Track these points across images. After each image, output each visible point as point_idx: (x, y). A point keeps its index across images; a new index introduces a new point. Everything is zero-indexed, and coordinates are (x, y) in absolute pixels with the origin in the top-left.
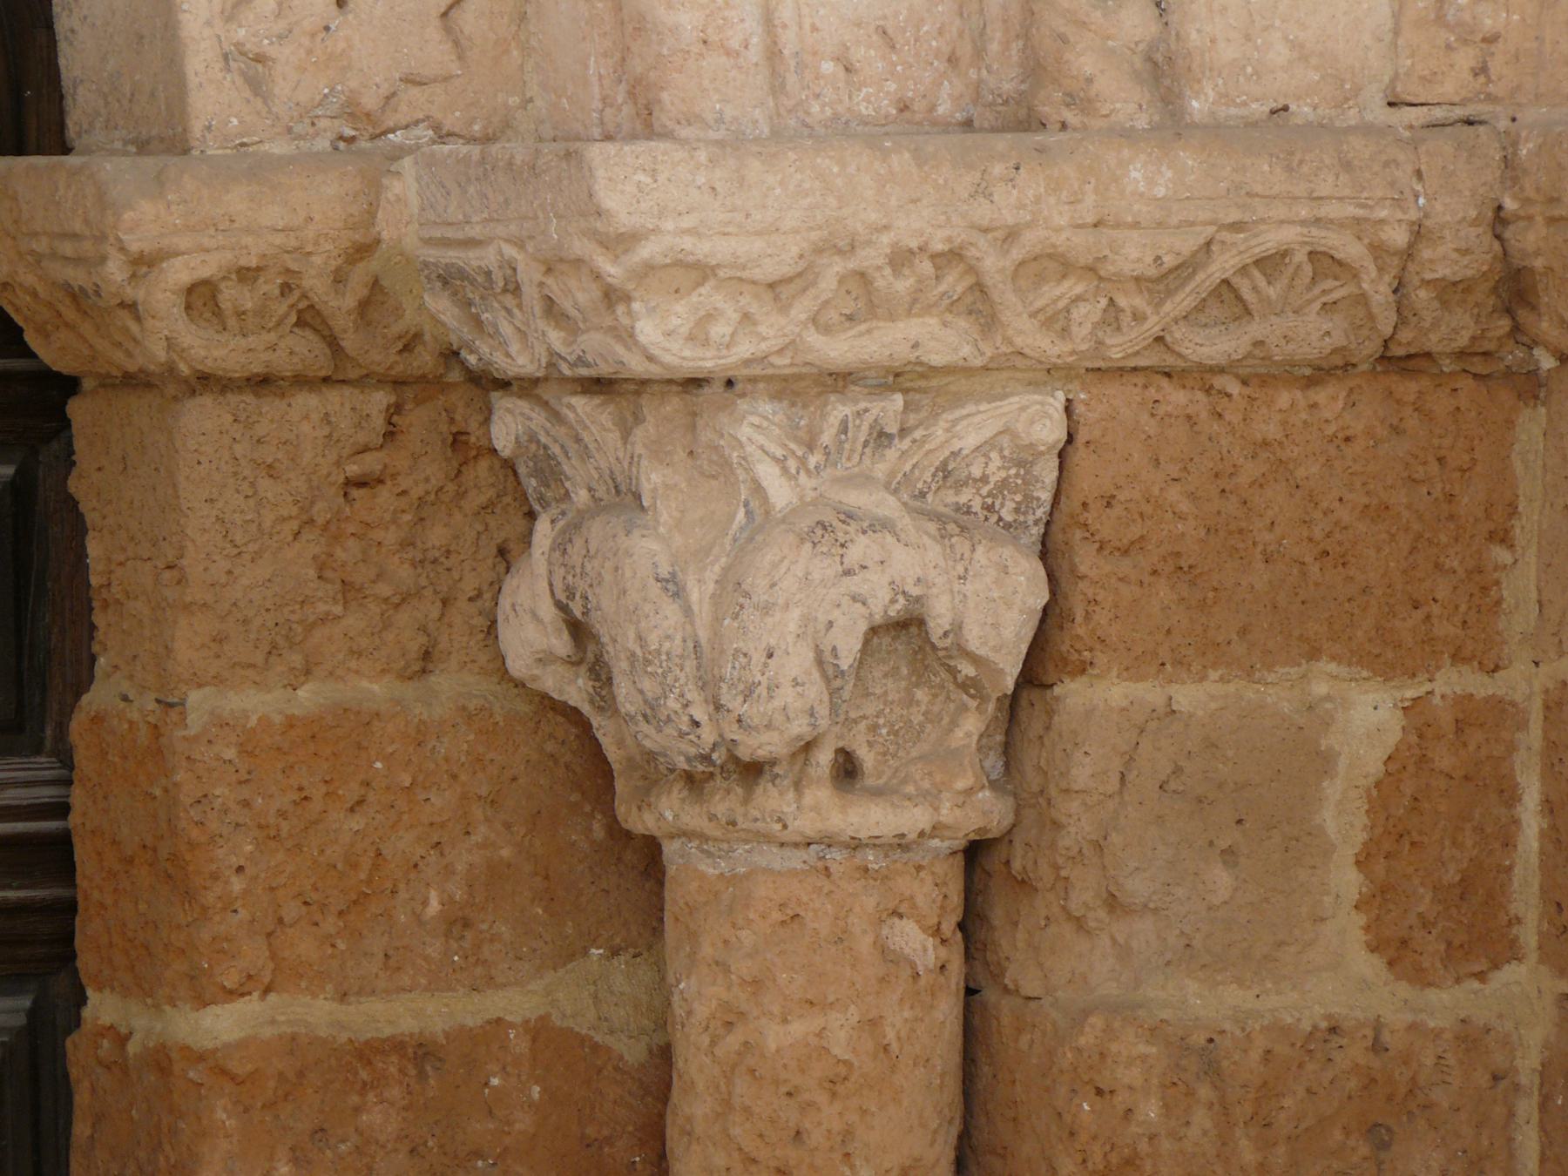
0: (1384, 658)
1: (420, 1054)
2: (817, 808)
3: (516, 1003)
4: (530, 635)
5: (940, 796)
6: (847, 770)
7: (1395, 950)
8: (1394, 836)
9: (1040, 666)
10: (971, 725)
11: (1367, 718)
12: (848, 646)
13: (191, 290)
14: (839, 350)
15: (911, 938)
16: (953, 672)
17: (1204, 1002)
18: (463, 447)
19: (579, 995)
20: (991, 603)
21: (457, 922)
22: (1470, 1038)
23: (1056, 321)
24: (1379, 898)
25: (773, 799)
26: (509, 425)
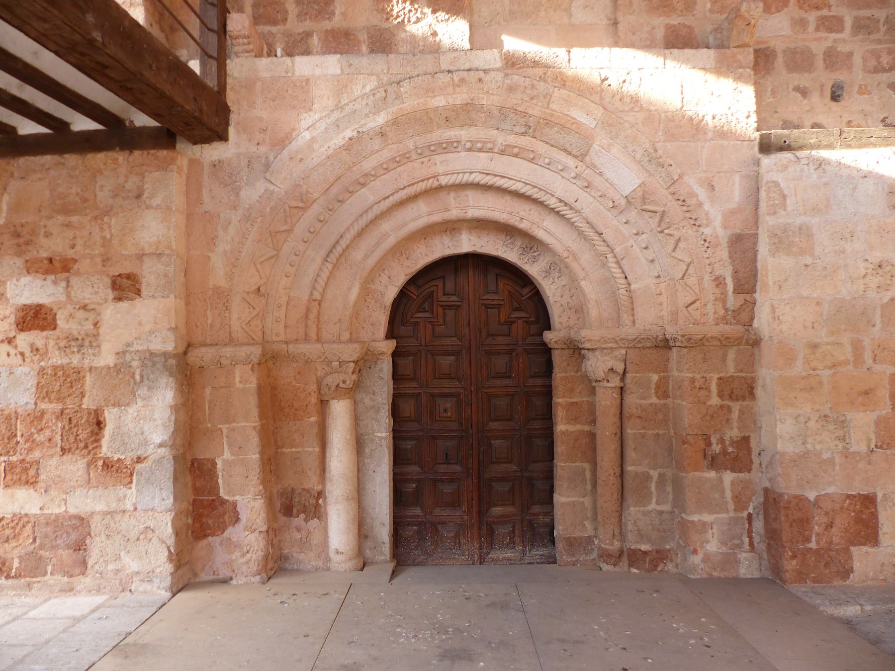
0: (656, 372)
1: (577, 403)
2: (606, 384)
3: (585, 399)
4: (583, 370)
5: (616, 382)
6: (608, 381)
7: (658, 398)
8: (658, 387)
9: (625, 373)
10: (619, 378)
11: (655, 378)
12: (606, 371)
13: (25, 308)
14: (603, 346)
15: (615, 395)
16: (245, 37)
17: (638, 401)
18: (580, 353)
19: (589, 399)
20: (620, 368)
21: (580, 393)
22: (665, 404)
23: (624, 344)
24: (656, 393)
25: (601, 384)
26: (583, 352)
